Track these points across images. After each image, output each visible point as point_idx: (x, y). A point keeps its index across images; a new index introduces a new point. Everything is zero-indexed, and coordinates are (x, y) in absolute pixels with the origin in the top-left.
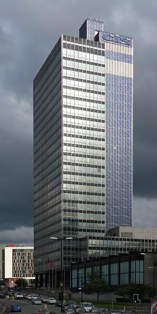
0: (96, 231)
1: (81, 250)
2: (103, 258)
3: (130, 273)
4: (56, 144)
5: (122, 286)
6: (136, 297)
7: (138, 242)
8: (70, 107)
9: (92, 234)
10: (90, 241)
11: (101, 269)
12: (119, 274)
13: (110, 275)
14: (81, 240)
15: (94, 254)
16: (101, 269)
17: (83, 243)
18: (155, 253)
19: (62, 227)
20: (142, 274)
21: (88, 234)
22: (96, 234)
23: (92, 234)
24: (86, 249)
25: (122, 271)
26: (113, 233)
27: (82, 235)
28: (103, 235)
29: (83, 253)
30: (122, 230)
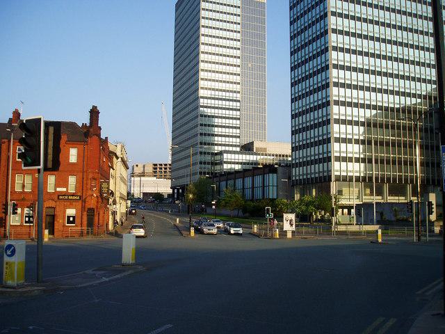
0: (232, 146)
1: (216, 164)
2: (237, 172)
3: (264, 186)
4: (194, 45)
5: (257, 200)
6: (268, 209)
7: (272, 157)
8: (206, 62)
9: (227, 148)
10: (225, 155)
11: (243, 182)
12: (253, 188)
13: (253, 188)
14: (216, 154)
15: (374, 116)
16: (243, 182)
17: (218, 157)
18: (58, 199)
19: (198, 161)
20: (275, 188)
21: (223, 148)
22: (231, 149)
23: (227, 148)
24: (221, 163)
25: (256, 185)
26: (247, 148)
27: (217, 149)
28: (238, 149)
29: (218, 167)
30: (257, 145)
